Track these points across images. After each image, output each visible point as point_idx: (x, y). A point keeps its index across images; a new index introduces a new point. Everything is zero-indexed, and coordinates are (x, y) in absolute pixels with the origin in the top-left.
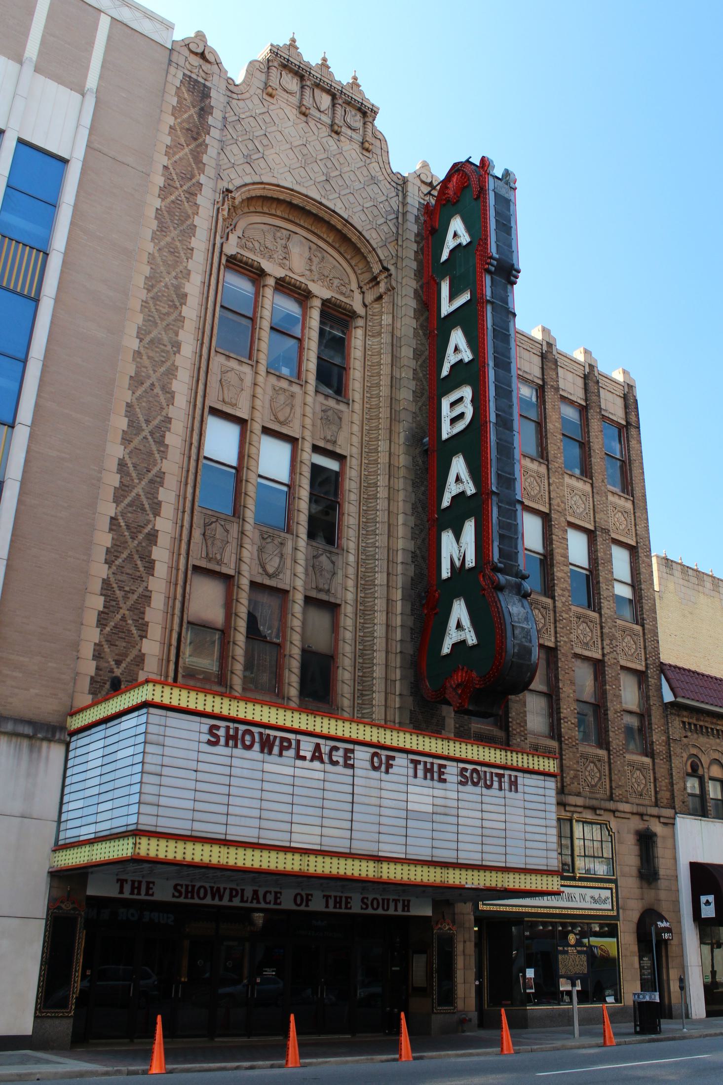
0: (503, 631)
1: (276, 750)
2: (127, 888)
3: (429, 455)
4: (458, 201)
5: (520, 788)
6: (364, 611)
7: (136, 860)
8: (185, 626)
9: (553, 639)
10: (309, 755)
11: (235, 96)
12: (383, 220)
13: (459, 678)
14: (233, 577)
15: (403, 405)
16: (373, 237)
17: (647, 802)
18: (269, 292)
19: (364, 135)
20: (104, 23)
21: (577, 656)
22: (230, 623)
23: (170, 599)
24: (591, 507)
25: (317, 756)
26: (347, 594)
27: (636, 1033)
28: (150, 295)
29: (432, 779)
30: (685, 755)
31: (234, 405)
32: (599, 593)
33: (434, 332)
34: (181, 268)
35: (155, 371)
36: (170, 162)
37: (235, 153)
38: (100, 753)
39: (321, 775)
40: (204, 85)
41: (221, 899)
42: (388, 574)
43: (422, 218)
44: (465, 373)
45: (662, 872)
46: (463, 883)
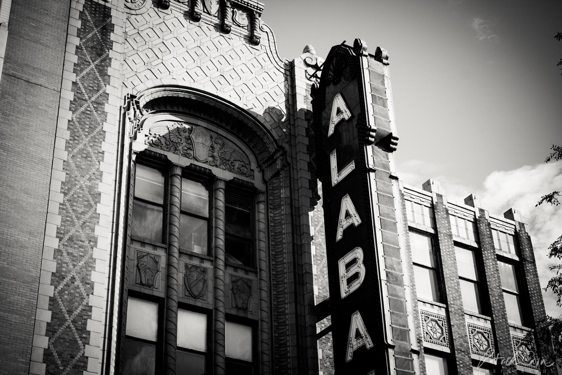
11: (133, 12)
31: (150, 286)
34: (94, 170)
36: (78, 78)
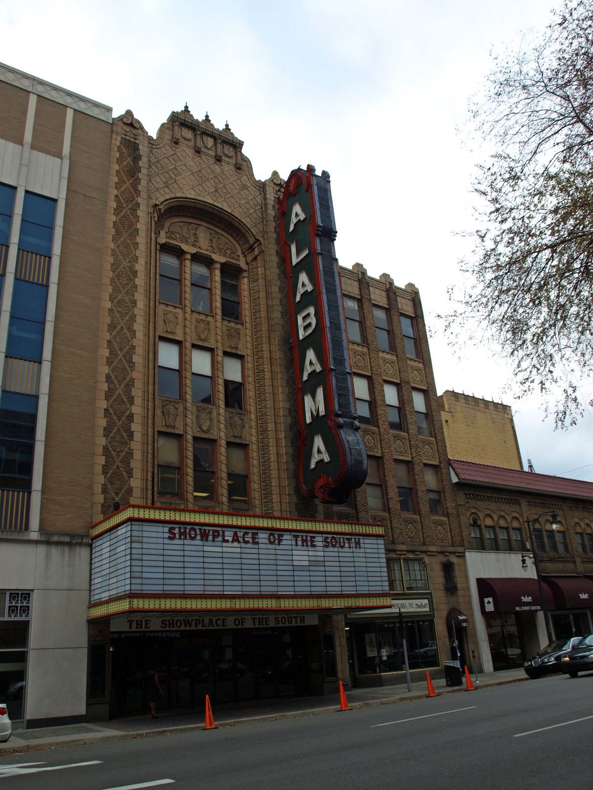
0: (344, 452)
1: (210, 538)
2: (134, 625)
3: (294, 350)
4: (295, 195)
5: (362, 545)
6: (264, 447)
7: (131, 611)
8: (156, 467)
9: (380, 452)
10: (230, 539)
11: (154, 147)
12: (253, 211)
13: (321, 482)
14: (182, 435)
15: (276, 321)
16: (246, 221)
17: (447, 544)
18: (188, 263)
19: (236, 160)
20: (70, 114)
21: (396, 460)
22: (183, 463)
23: (145, 453)
24: (397, 369)
25: (235, 539)
26: (251, 437)
27: (448, 685)
28: (115, 274)
29: (307, 545)
30: (468, 514)
32: (406, 421)
33: (289, 274)
35: (122, 319)
37: (158, 181)
38: (108, 549)
39: (239, 550)
40: (135, 143)
41: (190, 626)
42: (275, 423)
43: (277, 206)
44: (310, 298)
45: (459, 586)
46: (331, 605)
